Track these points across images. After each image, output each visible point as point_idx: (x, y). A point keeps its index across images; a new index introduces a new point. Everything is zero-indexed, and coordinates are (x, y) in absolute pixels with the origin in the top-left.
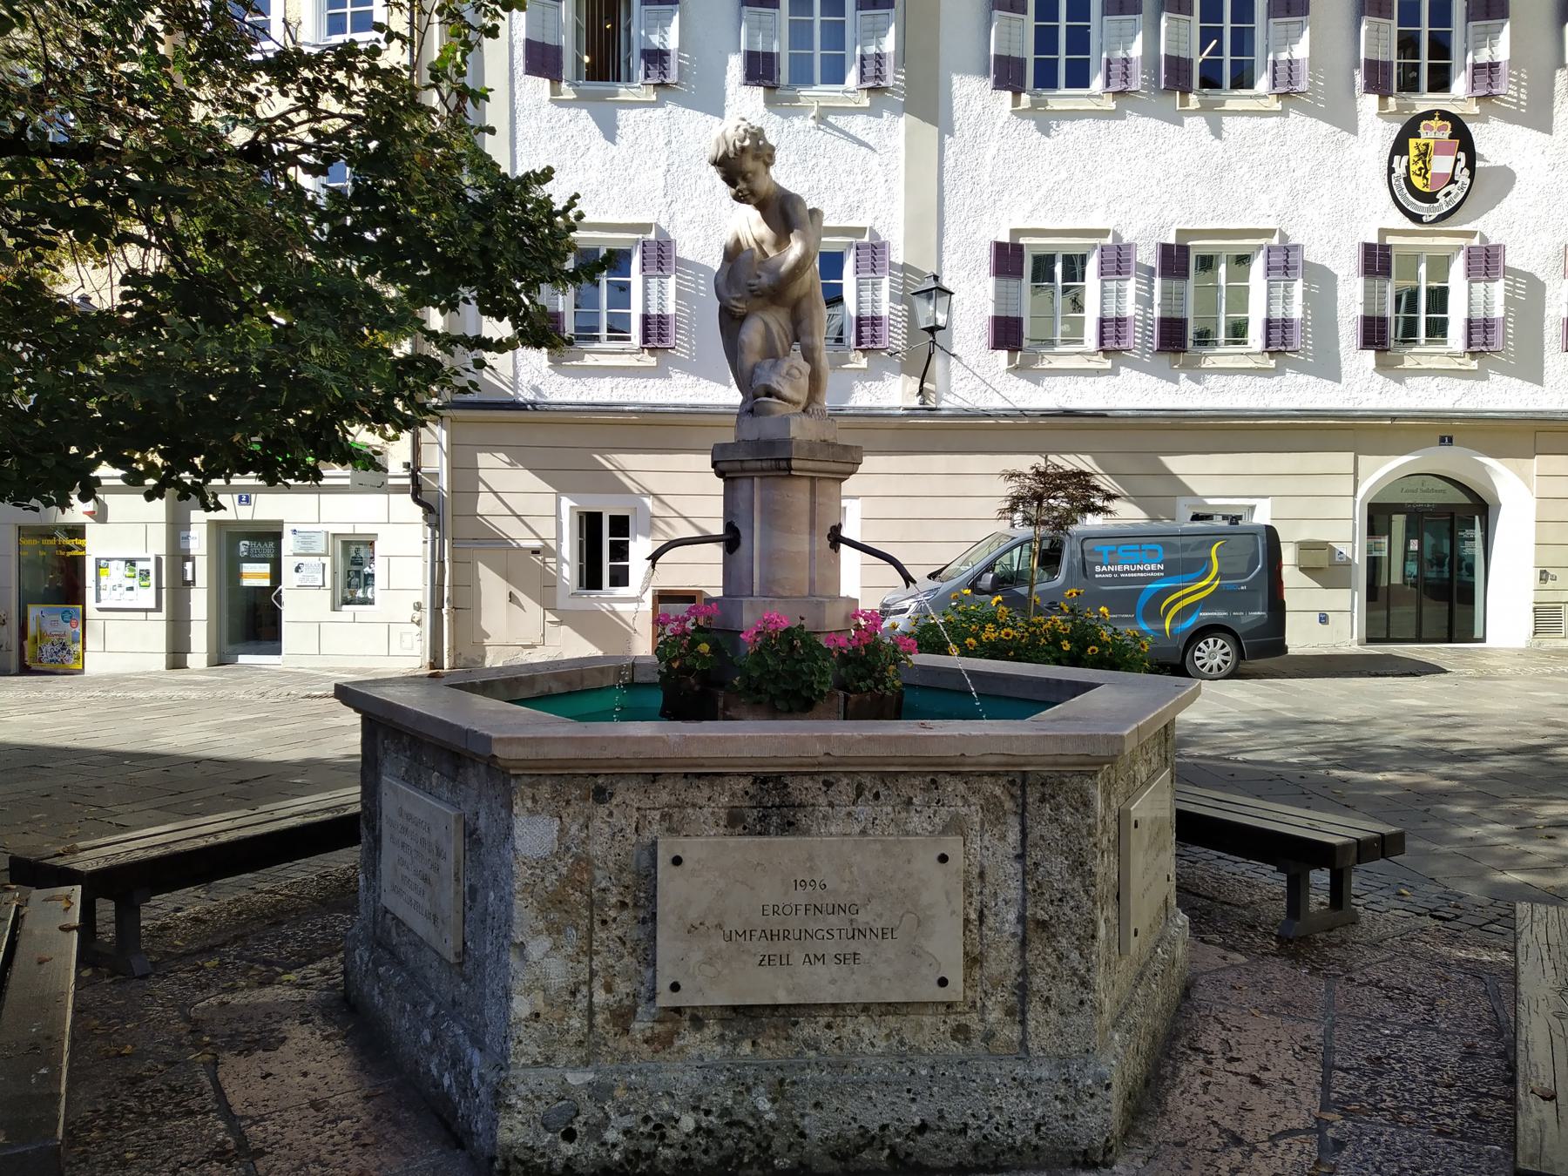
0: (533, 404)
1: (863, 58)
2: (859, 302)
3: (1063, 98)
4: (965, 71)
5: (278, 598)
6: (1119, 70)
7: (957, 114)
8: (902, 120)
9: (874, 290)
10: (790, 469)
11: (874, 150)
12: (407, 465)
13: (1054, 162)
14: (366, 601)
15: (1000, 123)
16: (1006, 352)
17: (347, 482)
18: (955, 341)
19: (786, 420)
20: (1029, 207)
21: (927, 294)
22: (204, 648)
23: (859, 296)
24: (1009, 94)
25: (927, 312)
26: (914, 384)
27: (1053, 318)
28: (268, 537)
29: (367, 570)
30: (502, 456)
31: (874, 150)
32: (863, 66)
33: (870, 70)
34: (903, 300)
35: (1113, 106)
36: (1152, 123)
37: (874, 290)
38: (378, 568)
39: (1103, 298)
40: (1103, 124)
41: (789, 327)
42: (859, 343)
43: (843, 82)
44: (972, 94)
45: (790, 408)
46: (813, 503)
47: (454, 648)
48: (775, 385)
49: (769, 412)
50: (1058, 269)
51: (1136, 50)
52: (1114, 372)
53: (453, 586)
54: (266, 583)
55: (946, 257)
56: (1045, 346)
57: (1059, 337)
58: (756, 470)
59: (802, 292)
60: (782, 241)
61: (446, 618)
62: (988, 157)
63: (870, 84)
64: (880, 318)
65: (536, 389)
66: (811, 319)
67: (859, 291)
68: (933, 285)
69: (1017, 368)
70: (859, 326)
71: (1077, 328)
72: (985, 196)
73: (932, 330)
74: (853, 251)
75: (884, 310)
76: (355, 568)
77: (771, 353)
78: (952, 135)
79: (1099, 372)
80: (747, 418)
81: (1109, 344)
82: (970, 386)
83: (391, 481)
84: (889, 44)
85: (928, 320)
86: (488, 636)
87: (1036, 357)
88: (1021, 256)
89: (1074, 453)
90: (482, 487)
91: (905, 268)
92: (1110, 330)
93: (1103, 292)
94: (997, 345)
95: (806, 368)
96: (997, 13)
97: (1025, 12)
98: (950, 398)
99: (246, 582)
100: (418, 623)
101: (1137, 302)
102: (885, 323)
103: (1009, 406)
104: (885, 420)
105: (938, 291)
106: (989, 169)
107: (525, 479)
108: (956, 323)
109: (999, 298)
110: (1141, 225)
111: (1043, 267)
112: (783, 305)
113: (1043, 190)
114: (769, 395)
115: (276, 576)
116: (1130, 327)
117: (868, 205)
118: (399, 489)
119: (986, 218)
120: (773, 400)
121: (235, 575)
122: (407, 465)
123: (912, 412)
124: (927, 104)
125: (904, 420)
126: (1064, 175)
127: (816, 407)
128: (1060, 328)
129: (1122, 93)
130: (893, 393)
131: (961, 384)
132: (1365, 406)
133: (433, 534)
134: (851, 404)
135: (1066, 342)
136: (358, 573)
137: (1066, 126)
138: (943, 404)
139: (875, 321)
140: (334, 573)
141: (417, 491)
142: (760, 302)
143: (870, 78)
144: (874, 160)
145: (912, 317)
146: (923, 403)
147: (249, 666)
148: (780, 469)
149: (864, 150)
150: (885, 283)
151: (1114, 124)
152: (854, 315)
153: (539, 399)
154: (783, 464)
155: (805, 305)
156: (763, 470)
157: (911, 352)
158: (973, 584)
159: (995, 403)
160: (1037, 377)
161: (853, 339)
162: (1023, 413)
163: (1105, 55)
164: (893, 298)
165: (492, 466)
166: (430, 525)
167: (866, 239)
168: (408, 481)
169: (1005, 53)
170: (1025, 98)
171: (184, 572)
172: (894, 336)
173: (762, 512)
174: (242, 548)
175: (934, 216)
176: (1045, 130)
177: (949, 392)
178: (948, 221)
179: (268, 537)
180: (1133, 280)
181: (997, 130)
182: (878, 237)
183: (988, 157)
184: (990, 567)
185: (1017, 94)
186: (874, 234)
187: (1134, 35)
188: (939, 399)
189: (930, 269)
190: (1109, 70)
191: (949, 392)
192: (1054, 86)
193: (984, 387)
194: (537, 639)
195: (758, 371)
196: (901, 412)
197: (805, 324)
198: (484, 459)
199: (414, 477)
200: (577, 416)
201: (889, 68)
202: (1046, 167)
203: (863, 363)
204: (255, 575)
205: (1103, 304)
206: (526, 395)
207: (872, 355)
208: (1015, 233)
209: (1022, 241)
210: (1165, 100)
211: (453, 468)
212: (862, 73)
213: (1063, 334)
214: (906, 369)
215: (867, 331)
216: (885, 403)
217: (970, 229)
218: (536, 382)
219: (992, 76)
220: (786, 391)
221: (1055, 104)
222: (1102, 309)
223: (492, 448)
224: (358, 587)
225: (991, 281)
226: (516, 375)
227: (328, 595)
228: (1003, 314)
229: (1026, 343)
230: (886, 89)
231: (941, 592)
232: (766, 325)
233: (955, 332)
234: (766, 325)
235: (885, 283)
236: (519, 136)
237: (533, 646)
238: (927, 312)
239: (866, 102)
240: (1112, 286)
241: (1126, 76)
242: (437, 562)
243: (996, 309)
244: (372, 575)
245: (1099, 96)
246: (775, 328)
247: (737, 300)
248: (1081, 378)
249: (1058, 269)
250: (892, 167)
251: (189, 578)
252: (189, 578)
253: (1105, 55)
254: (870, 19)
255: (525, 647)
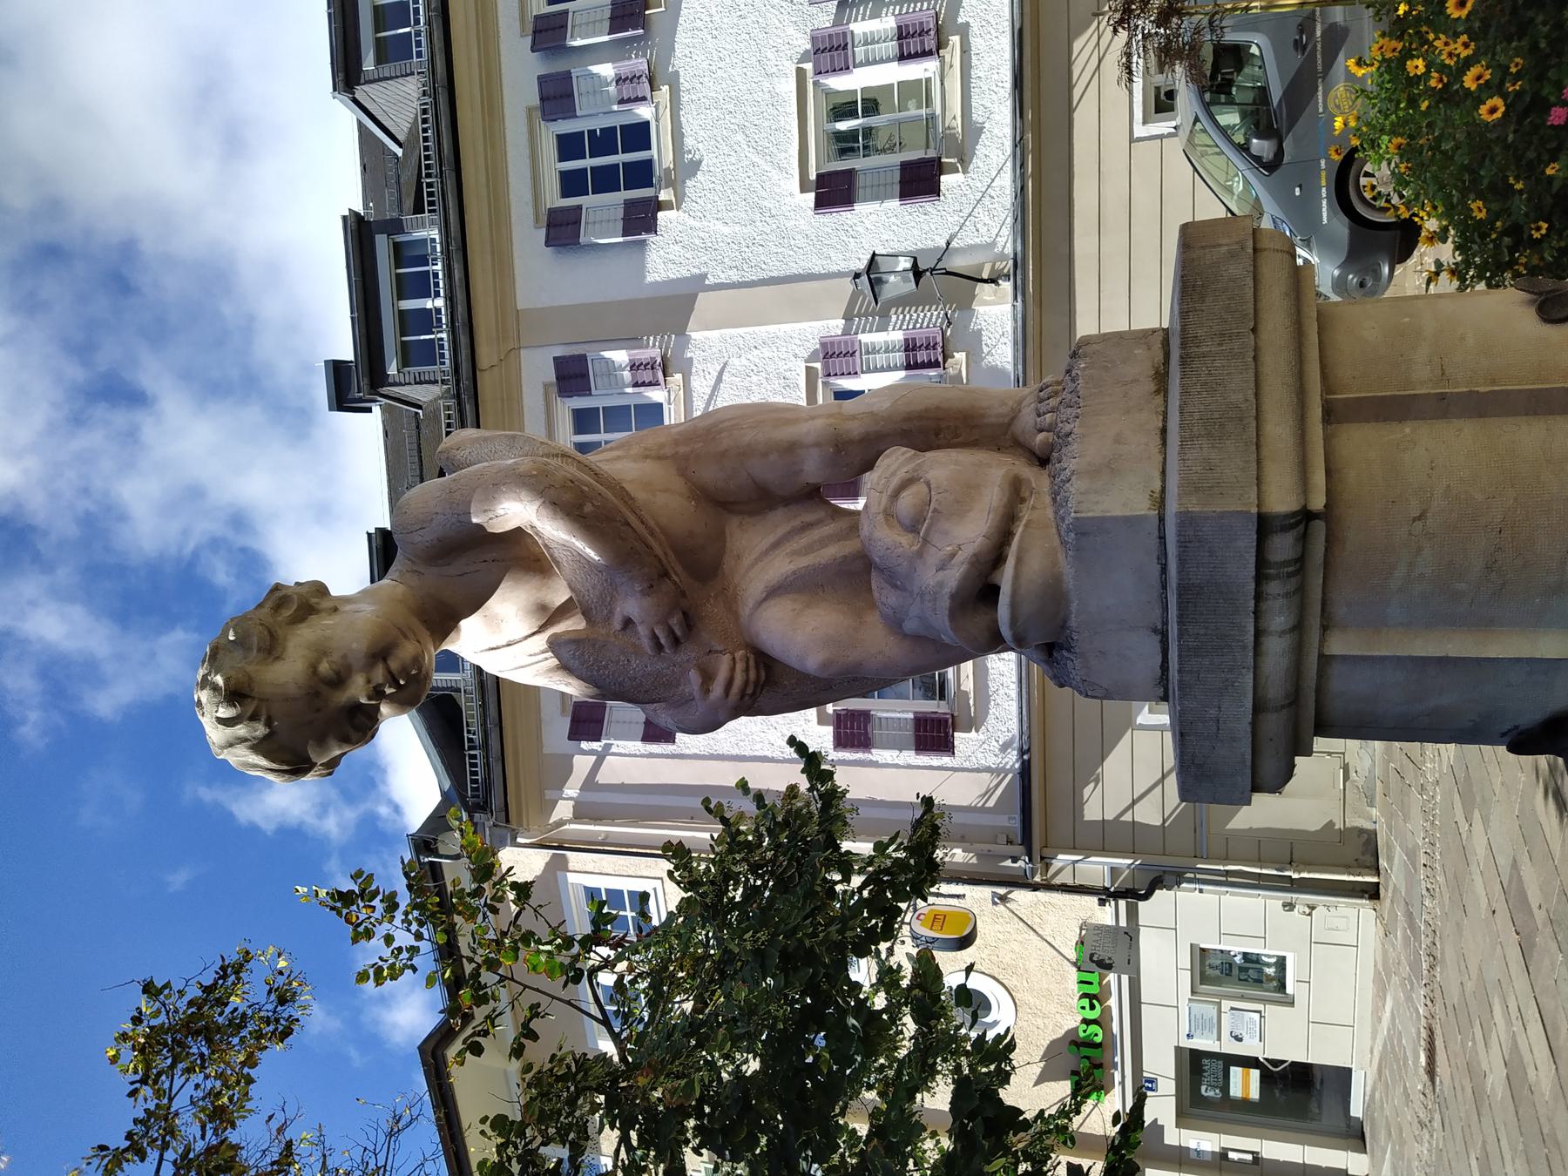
0: (1022, 752)
1: (636, 385)
2: (889, 369)
3: (662, 153)
4: (641, 269)
5: (1276, 1063)
6: (632, 88)
7: (685, 273)
8: (694, 335)
9: (875, 351)
10: (1306, 516)
11: (726, 364)
12: (1102, 903)
13: (727, 150)
14: (1281, 963)
15: (691, 222)
16: (943, 178)
17: (1125, 978)
18: (930, 244)
19: (1085, 536)
20: (775, 174)
21: (876, 284)
22: (1341, 1154)
23: (882, 369)
24: (660, 215)
25: (896, 284)
26: (984, 291)
27: (900, 123)
28: (1193, 1064)
29: (1238, 959)
30: (1087, 791)
31: (726, 364)
32: (643, 384)
33: (646, 376)
34: (885, 315)
35: (665, 88)
36: (682, 38)
37: (875, 351)
38: (1236, 948)
39: (875, 62)
40: (685, 98)
41: (780, 522)
42: (935, 364)
43: (661, 405)
44: (669, 254)
45: (1037, 510)
46: (1444, 406)
47: (1347, 868)
48: (953, 577)
49: (1054, 597)
50: (843, 126)
51: (606, 70)
52: (964, 31)
53: (1259, 862)
54: (1255, 1074)
55: (835, 268)
56: (935, 127)
57: (923, 111)
58: (1298, 651)
59: (678, 484)
60: (518, 555)
61: (1305, 875)
62: (726, 230)
63: (660, 374)
64: (906, 340)
65: (1005, 747)
66: (745, 453)
67: (876, 370)
68: (865, 278)
69: (962, 161)
70: (917, 366)
71: (915, 91)
72: (767, 229)
73: (917, 273)
74: (832, 380)
75: (897, 336)
76: (1235, 971)
77: (856, 576)
78: (705, 276)
79: (965, 50)
80: (1076, 668)
81: (930, 43)
82: (986, 219)
83: (1123, 923)
84: (620, 356)
85: (905, 280)
86: (1331, 824)
87: (949, 136)
88: (830, 174)
89: (1070, 64)
90: (1127, 817)
91: (848, 317)
92: (913, 45)
93: (868, 63)
94: (933, 190)
95: (895, 462)
96: (581, 240)
97: (579, 207)
98: (1001, 241)
99: (1254, 1094)
100: (1313, 908)
101: (879, 16)
102: (912, 333)
103: (1009, 164)
104: (1030, 323)
105: (873, 271)
106: (737, 228)
107: (1115, 765)
108: (909, 246)
109: (880, 197)
110: (791, 30)
111: (845, 144)
112: (719, 538)
113: (755, 159)
114: (989, 593)
115: (1249, 1062)
116: (909, 19)
117: (782, 366)
118: (1133, 914)
119: (790, 224)
120: (1005, 578)
121: (1244, 1105)
122: (1102, 903)
123: (1019, 290)
124: (674, 308)
125: (1030, 300)
126: (740, 137)
127: (1028, 418)
128: (913, 112)
129: (651, 81)
130: (995, 315)
131: (983, 230)
132: (1007, 55)
133: (1190, 881)
134: (1010, 367)
135: (929, 103)
136: (1242, 969)
137: (689, 142)
138: (1009, 250)
139: (910, 346)
140: (1243, 998)
141: (1132, 893)
142: (713, 609)
143: (654, 375)
144: (735, 361)
145: (903, 302)
146: (1007, 277)
147: (1368, 1108)
148: (1301, 562)
149: (726, 376)
150: (865, 338)
151: (684, 84)
152: (903, 374)
153: (1016, 745)
154: (1282, 547)
155: (709, 474)
156: (1298, 628)
157: (946, 299)
158: (1270, 167)
159: (1006, 182)
160: (973, 131)
161: (932, 372)
162: (1019, 143)
163: (615, 108)
164: (882, 328)
165: (1100, 803)
166: (1178, 884)
167: (818, 365)
168: (1122, 903)
169: (620, 225)
170: (664, 195)
171: (1240, 1162)
172: (928, 320)
173: (1485, 623)
174: (1211, 1094)
175: (787, 288)
176: (695, 166)
177: (994, 244)
178: (795, 269)
179: (1193, 1064)
180: (852, 26)
181: (697, 224)
182: (815, 352)
183: (726, 230)
184: (1244, 149)
185: (660, 206)
186: (812, 357)
187: (593, 76)
188: (1002, 257)
189: (847, 285)
190: (629, 101)
191: (994, 244)
192: (649, 163)
193: (986, 200)
194: (1336, 762)
195: (910, 625)
196: (1019, 304)
197: (767, 471)
198: (1092, 812)
199: (1116, 895)
200: (1036, 701)
201: (644, 355)
202: (733, 160)
203: (960, 356)
204: (1246, 1084)
205: (882, 61)
206: (1012, 759)
207: (950, 347)
208: (804, 189)
209: (813, 177)
210: (657, 27)
211: (1103, 850)
212: (650, 384)
213: (919, 107)
214: (966, 303)
215: (922, 356)
216: (1009, 327)
217: (801, 242)
218: (995, 746)
219: (644, 236)
220: (970, 533)
221: (668, 160)
222: (889, 60)
223: (1077, 805)
224: (1261, 971)
225: (859, 208)
226: (988, 770)
227: (1271, 1010)
228: (897, 188)
229: (931, 154)
230: (664, 358)
231: (1279, 214)
232: (774, 592)
233: (920, 246)
234: (774, 592)
235: (865, 338)
236: (735, 752)
237: (1346, 768)
238: (896, 284)
239: (678, 377)
240: (860, 52)
241: (633, 78)
242: (1227, 880)
243: (893, 197)
244: (1245, 955)
245: (657, 108)
246: (781, 566)
247: (707, 678)
248: (974, 73)
249: (843, 126)
250: (741, 342)
251: (1249, 1157)
252: (1249, 1157)
253: (615, 108)
254: (599, 380)
255: (1346, 777)
